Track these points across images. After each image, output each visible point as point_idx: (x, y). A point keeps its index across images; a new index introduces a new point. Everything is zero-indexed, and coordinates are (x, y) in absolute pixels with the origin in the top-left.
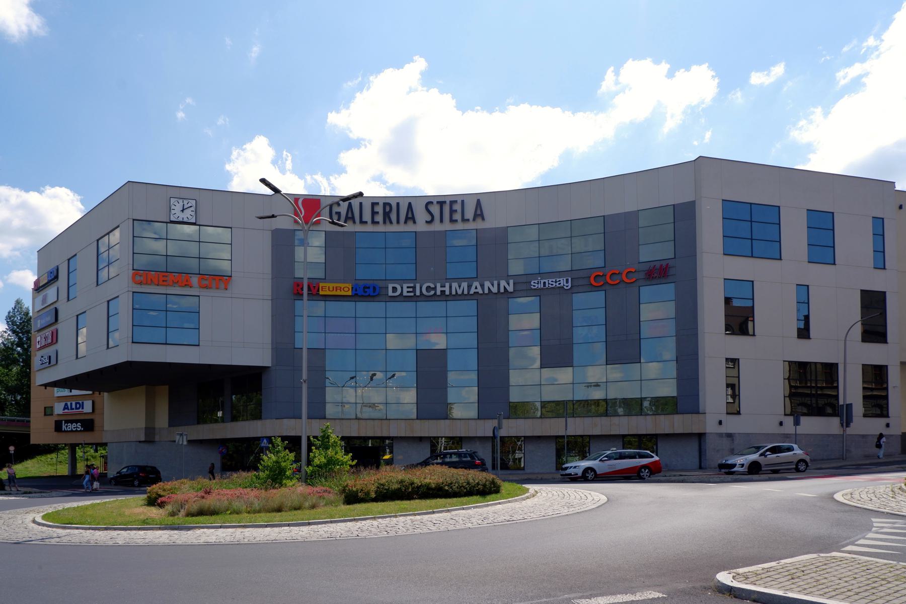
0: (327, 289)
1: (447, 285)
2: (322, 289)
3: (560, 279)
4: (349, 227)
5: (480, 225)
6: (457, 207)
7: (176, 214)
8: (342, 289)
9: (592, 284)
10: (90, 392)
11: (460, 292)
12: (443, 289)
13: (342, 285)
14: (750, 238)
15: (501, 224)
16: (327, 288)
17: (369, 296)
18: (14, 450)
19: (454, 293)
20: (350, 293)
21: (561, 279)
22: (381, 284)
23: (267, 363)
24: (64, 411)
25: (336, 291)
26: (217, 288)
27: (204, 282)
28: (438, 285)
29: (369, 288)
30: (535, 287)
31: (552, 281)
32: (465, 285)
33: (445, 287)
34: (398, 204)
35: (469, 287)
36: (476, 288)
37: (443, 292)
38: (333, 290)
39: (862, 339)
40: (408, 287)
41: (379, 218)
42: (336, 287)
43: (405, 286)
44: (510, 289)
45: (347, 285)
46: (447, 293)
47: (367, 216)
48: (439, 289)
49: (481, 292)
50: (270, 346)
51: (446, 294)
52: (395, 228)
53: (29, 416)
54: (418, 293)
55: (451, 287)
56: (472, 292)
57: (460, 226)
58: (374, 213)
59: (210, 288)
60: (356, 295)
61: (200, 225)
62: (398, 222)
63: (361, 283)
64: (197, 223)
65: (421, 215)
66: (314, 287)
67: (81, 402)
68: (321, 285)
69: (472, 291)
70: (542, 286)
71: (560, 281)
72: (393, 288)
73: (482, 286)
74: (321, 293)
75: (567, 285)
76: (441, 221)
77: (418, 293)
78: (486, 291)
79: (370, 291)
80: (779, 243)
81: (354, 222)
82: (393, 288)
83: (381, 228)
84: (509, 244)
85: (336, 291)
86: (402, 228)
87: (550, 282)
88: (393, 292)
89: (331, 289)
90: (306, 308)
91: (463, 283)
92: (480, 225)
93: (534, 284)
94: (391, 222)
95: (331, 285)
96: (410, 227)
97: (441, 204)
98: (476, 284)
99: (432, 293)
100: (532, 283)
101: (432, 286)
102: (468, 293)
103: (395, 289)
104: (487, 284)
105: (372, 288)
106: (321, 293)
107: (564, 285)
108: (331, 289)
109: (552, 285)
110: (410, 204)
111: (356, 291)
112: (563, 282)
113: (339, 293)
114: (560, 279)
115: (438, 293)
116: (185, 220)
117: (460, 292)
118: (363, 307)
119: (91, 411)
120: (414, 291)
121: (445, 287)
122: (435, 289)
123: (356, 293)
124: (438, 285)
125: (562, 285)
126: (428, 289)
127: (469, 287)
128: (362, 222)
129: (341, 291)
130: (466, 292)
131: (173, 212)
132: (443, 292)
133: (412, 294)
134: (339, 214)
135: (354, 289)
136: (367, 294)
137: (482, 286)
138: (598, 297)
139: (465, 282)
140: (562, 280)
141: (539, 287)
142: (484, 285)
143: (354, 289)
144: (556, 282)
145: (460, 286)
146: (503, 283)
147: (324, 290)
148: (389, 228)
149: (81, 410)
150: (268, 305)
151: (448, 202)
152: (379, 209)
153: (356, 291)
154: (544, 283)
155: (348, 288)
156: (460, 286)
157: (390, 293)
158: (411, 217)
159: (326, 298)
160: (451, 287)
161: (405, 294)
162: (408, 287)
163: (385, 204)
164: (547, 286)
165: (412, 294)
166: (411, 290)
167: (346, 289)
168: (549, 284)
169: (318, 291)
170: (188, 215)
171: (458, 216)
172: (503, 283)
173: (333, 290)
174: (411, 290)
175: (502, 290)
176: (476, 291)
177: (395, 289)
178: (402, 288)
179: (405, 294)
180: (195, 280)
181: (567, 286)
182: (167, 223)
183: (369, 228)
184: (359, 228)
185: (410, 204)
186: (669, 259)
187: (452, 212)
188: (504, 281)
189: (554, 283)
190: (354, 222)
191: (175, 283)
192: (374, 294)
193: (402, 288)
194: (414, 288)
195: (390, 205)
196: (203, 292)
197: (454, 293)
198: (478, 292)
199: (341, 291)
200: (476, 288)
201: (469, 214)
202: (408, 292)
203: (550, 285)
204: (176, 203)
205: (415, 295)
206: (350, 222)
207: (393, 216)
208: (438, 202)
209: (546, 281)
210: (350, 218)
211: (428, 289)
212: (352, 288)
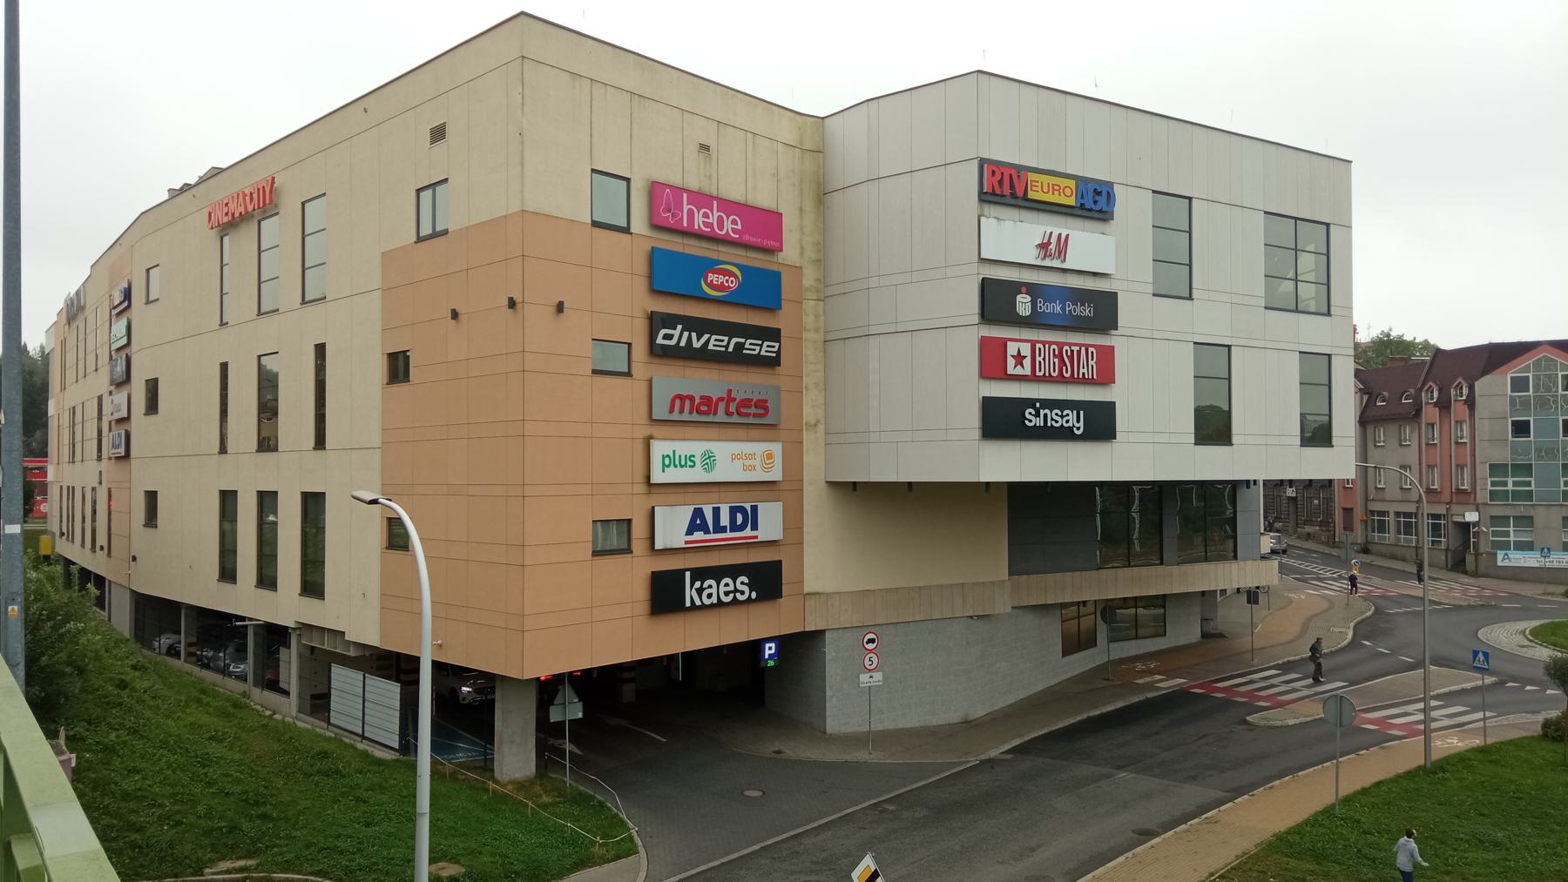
20: (1072, 201)
53: (1216, 591)
107: (1074, 426)
111: (1082, 197)
125: (1070, 424)
153: (1082, 197)
159: (733, 571)
168: (1052, 419)
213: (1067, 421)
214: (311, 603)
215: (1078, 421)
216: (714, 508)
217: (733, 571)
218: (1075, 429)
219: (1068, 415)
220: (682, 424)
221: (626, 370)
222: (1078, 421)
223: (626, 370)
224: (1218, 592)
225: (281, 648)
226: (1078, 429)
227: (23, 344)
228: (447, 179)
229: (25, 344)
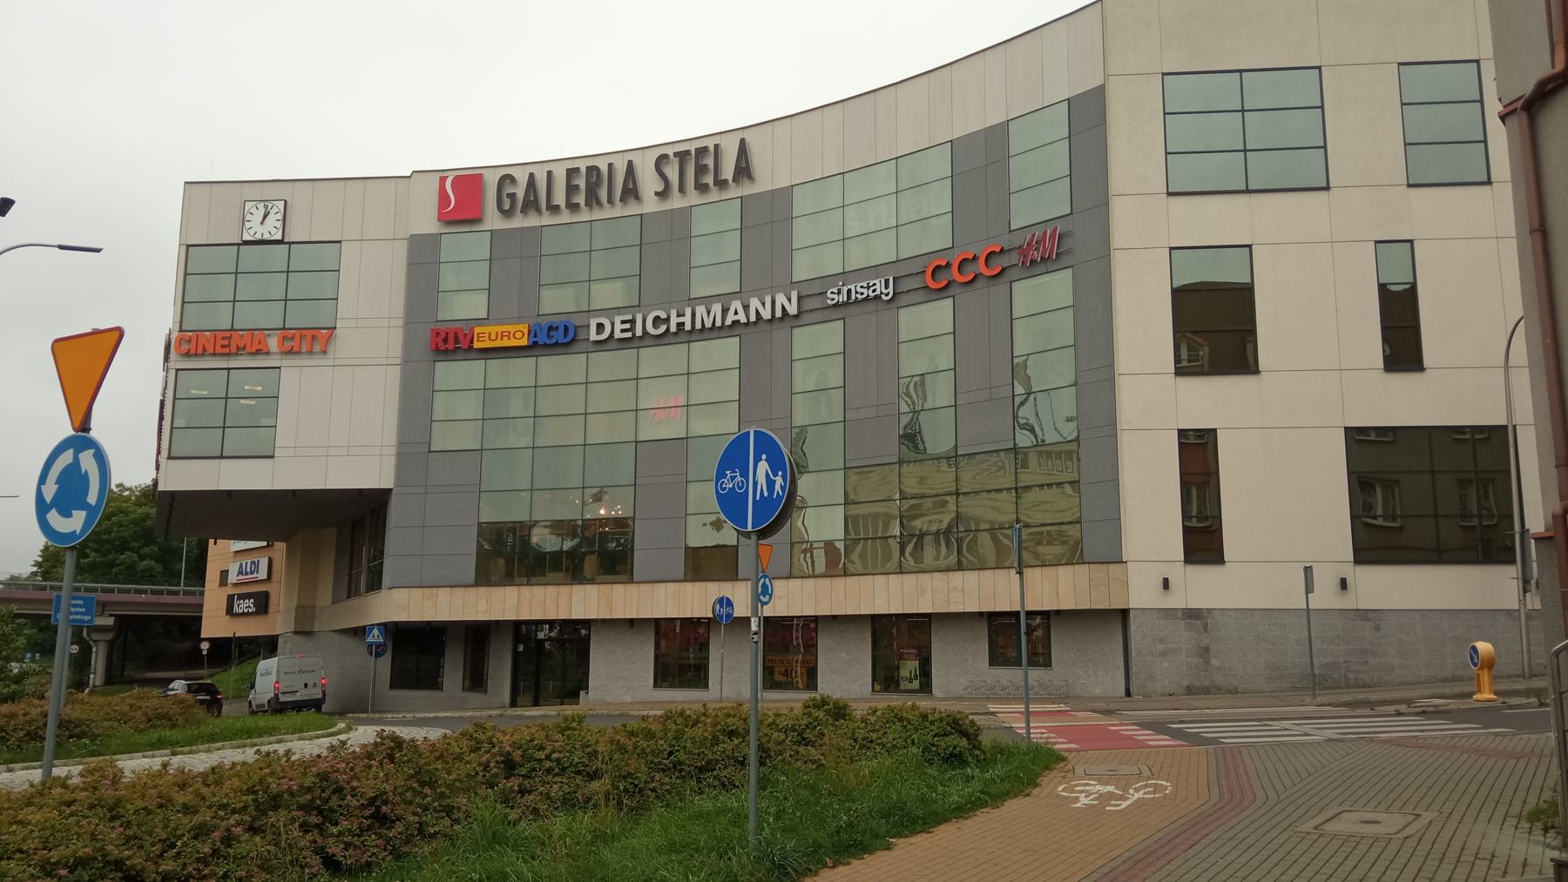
0: (487, 338)
1: (688, 312)
2: (478, 337)
3: (874, 282)
4: (532, 221)
5: (748, 190)
6: (710, 162)
7: (256, 230)
8: (511, 335)
9: (927, 287)
10: (265, 543)
11: (708, 324)
12: (681, 320)
13: (511, 328)
14: (286, 274)
15: (782, 183)
16: (487, 335)
17: (556, 344)
18: (208, 650)
19: (698, 326)
20: (524, 342)
21: (877, 282)
22: (578, 321)
23: (386, 482)
24: (238, 578)
25: (502, 339)
26: (310, 352)
27: (288, 344)
28: (673, 313)
29: (557, 328)
30: (835, 302)
31: (862, 287)
32: (717, 308)
33: (684, 315)
34: (550, 174)
35: (725, 311)
36: (736, 313)
37: (681, 325)
38: (497, 338)
39: (1386, 358)
40: (623, 322)
41: (580, 199)
42: (502, 332)
43: (618, 320)
44: (792, 309)
45: (520, 327)
46: (688, 327)
47: (560, 198)
48: (674, 320)
49: (743, 320)
50: (393, 451)
51: (686, 329)
52: (607, 212)
53: (204, 587)
54: (639, 332)
55: (693, 315)
56: (728, 322)
57: (714, 195)
58: (571, 189)
59: (299, 353)
60: (534, 346)
61: (290, 243)
62: (610, 200)
63: (545, 321)
64: (286, 240)
65: (649, 183)
66: (466, 334)
67: (256, 560)
68: (477, 330)
69: (730, 318)
70: (845, 299)
71: (874, 284)
72: (598, 324)
73: (746, 307)
74: (476, 345)
75: (887, 291)
76: (682, 190)
77: (639, 332)
78: (753, 318)
79: (558, 336)
80: (1483, 144)
81: (538, 210)
82: (598, 324)
83: (584, 216)
84: (692, 239)
85: (502, 339)
86: (618, 211)
87: (859, 289)
88: (598, 334)
89: (493, 337)
90: (455, 374)
91: (714, 305)
92: (748, 190)
93: (833, 296)
94: (599, 203)
95: (494, 329)
96: (633, 209)
97: (682, 156)
98: (736, 304)
99: (663, 328)
100: (829, 295)
101: (663, 315)
102: (723, 323)
103: (600, 327)
104: (755, 303)
105: (561, 329)
106: (476, 345)
107: (882, 293)
108: (493, 337)
109: (862, 294)
110: (630, 163)
111: (535, 336)
112: (879, 286)
113: (506, 343)
114: (874, 282)
115: (673, 329)
116: (267, 236)
117: (708, 324)
118: (552, 366)
119: (265, 577)
120: (632, 329)
121: (684, 315)
122: (668, 320)
123: (535, 340)
124: (673, 313)
125: (878, 292)
126: (657, 321)
127: (725, 311)
128: (554, 209)
129: (509, 339)
130: (718, 323)
131: (248, 225)
132: (681, 325)
133: (629, 335)
134: (512, 196)
135: (532, 333)
136: (553, 341)
137: (746, 307)
138: (940, 314)
139: (701, 304)
140: (878, 284)
141: (841, 300)
142: (749, 306)
143: (532, 334)
144: (868, 287)
145: (709, 312)
146: (781, 299)
147: (480, 339)
148: (598, 215)
149: (255, 575)
150: (396, 372)
151: (583, 170)
152: (581, 182)
153: (535, 336)
154: (849, 291)
155: (523, 332)
156: (709, 312)
157: (593, 336)
158: (631, 191)
159: (487, 353)
160: (693, 315)
161: (618, 335)
162: (623, 322)
163: (591, 169)
164: (853, 298)
165: (629, 335)
166: (627, 326)
167: (519, 335)
168: (857, 292)
169: (472, 341)
170: (271, 229)
171: (709, 179)
172: (781, 299)
173: (497, 338)
174: (627, 326)
175: (779, 314)
176: (736, 318)
177: (600, 327)
178: (613, 324)
179: (618, 335)
180: (273, 343)
181: (887, 295)
182: (238, 245)
183: (566, 217)
184: (547, 219)
185: (630, 163)
186: (1025, 227)
187: (701, 170)
188: (782, 294)
189: (865, 291)
190: (538, 210)
191: (241, 350)
192: (568, 339)
193: (613, 324)
194: (632, 322)
195: (596, 168)
196: (283, 362)
197: (698, 326)
198: (739, 321)
199: (509, 339)
200: (736, 313)
201: (728, 172)
202: (623, 331)
203: (858, 296)
204: (254, 210)
205: (634, 335)
206: (532, 213)
207: (603, 194)
208: (676, 154)
209: (852, 287)
210: (531, 204)
211: (657, 321)
212: (529, 331)
213: (874, 291)
214: (560, 328)
215: (886, 288)
216: (52, 600)
217: (487, 353)
218: (882, 296)
219: (874, 284)
220: (178, 319)
221: (1325, 185)
222: (886, 288)
223: (1325, 185)
224: (202, 589)
225: (54, 510)
226: (887, 295)
227: (83, 471)
228: (565, 326)
229: (86, 471)
